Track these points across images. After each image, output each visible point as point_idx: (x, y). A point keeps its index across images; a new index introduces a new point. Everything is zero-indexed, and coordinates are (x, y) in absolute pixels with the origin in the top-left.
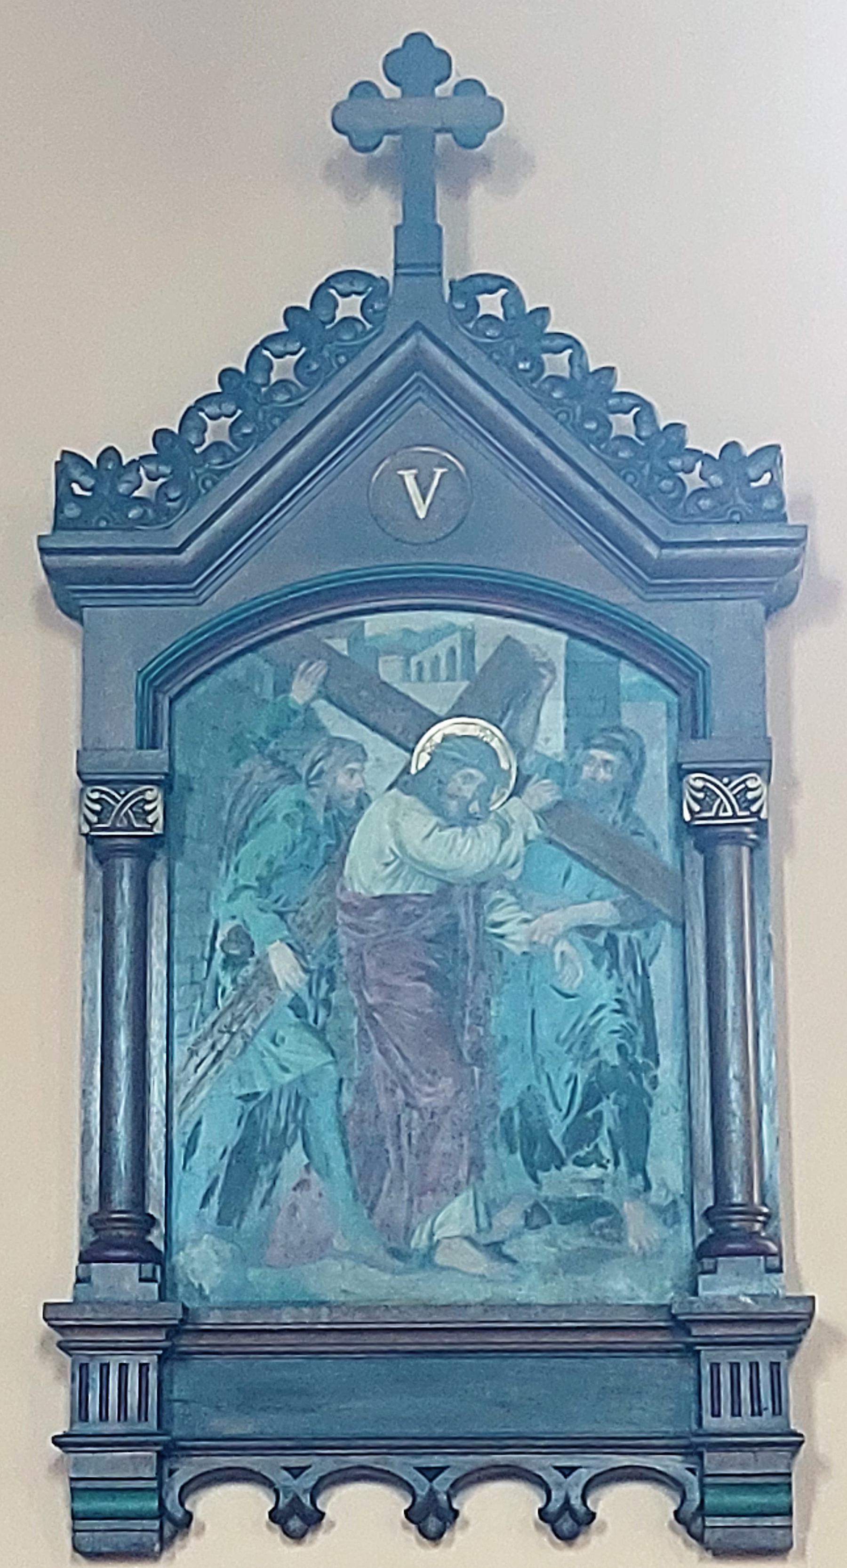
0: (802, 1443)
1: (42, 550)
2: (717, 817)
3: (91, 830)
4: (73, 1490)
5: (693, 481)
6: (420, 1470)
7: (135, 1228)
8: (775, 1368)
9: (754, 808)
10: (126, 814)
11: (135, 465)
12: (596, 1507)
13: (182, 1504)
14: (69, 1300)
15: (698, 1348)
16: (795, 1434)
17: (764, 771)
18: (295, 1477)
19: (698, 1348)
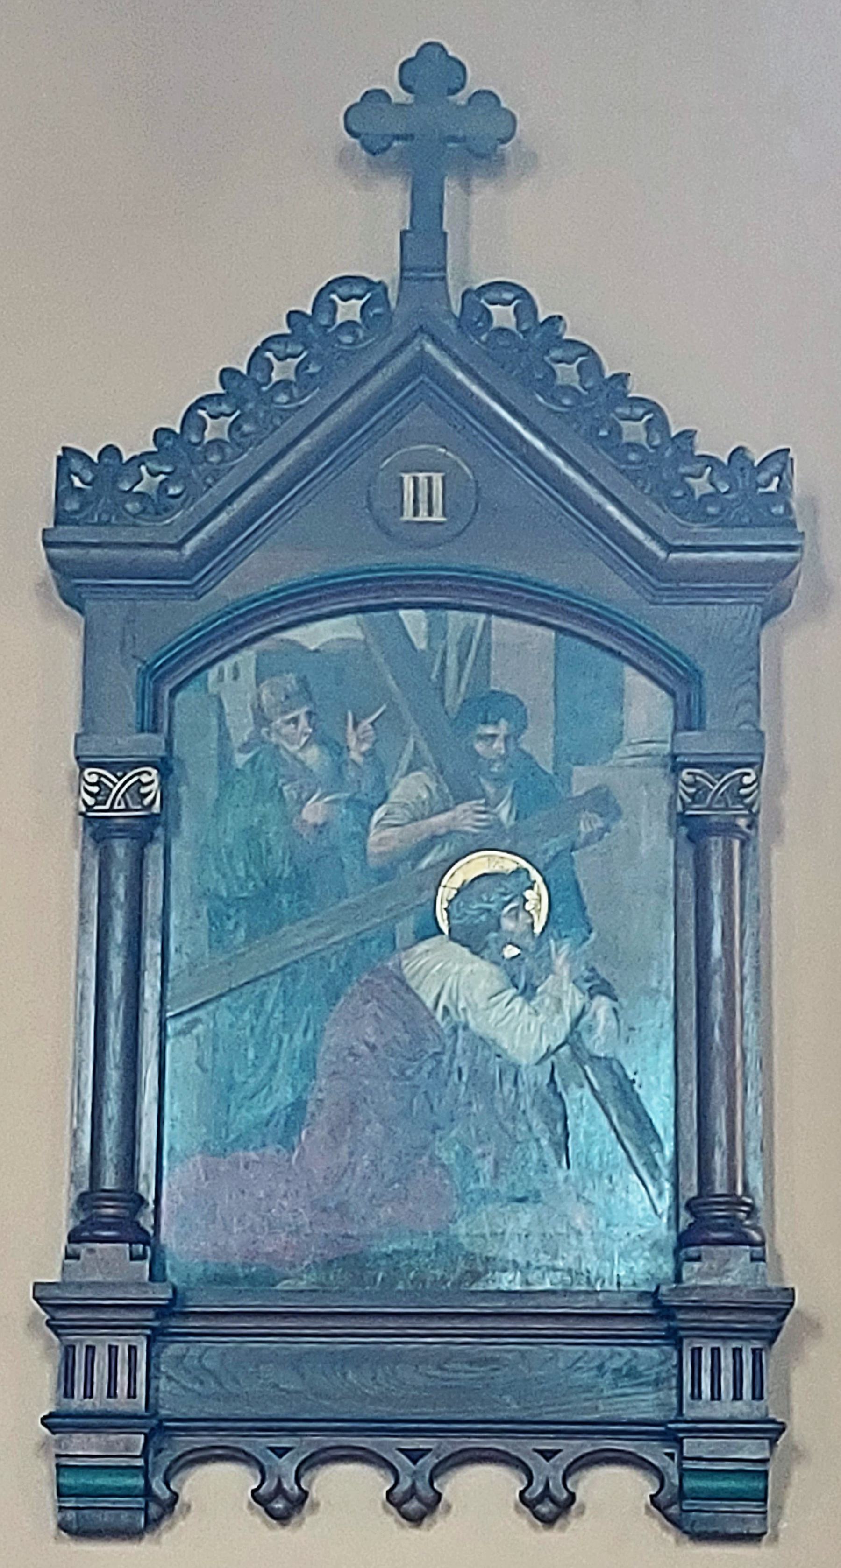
0: (784, 1430)
1: (47, 544)
2: (111, 809)
3: (87, 811)
4: (58, 1466)
5: (701, 486)
7: (124, 1208)
9: (147, 801)
11: (135, 462)
13: (167, 1484)
14: (57, 1279)
16: (773, 1421)
18: (548, 1459)
19: (682, 1333)
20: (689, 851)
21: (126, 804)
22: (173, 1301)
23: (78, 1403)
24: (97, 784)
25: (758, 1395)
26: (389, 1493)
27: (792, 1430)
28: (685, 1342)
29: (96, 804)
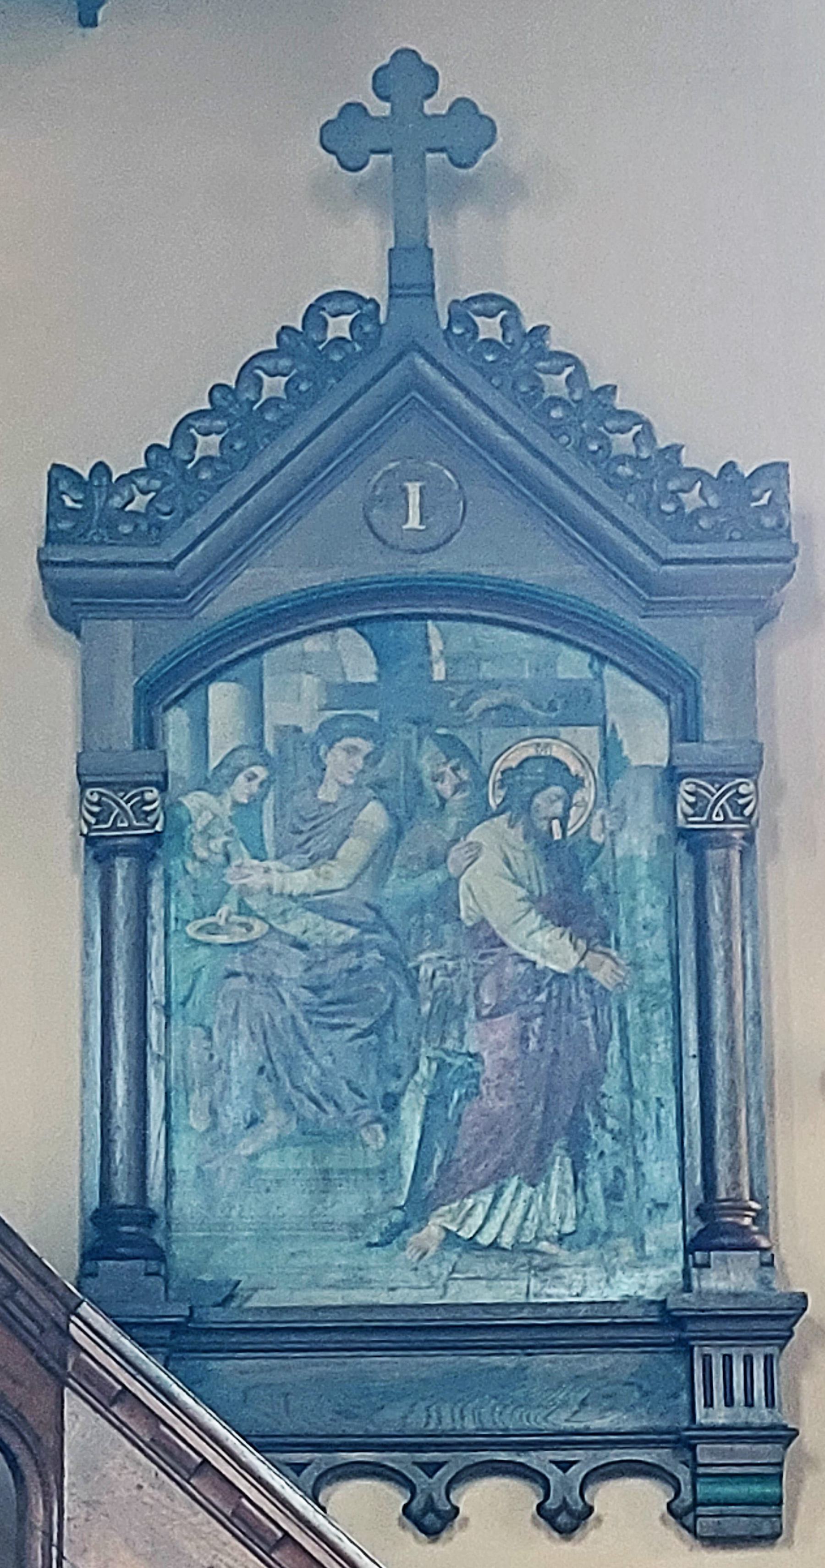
0: (798, 1434)
5: (692, 500)
8: (748, 1359)
10: (722, 806)
12: (458, 1501)
15: (692, 1343)
16: (785, 1428)
19: (692, 1343)
20: (96, 871)
22: (190, 1318)
24: (98, 804)
25: (770, 1403)
26: (406, 1507)
27: (803, 1437)
28: (696, 1349)
29: (97, 823)
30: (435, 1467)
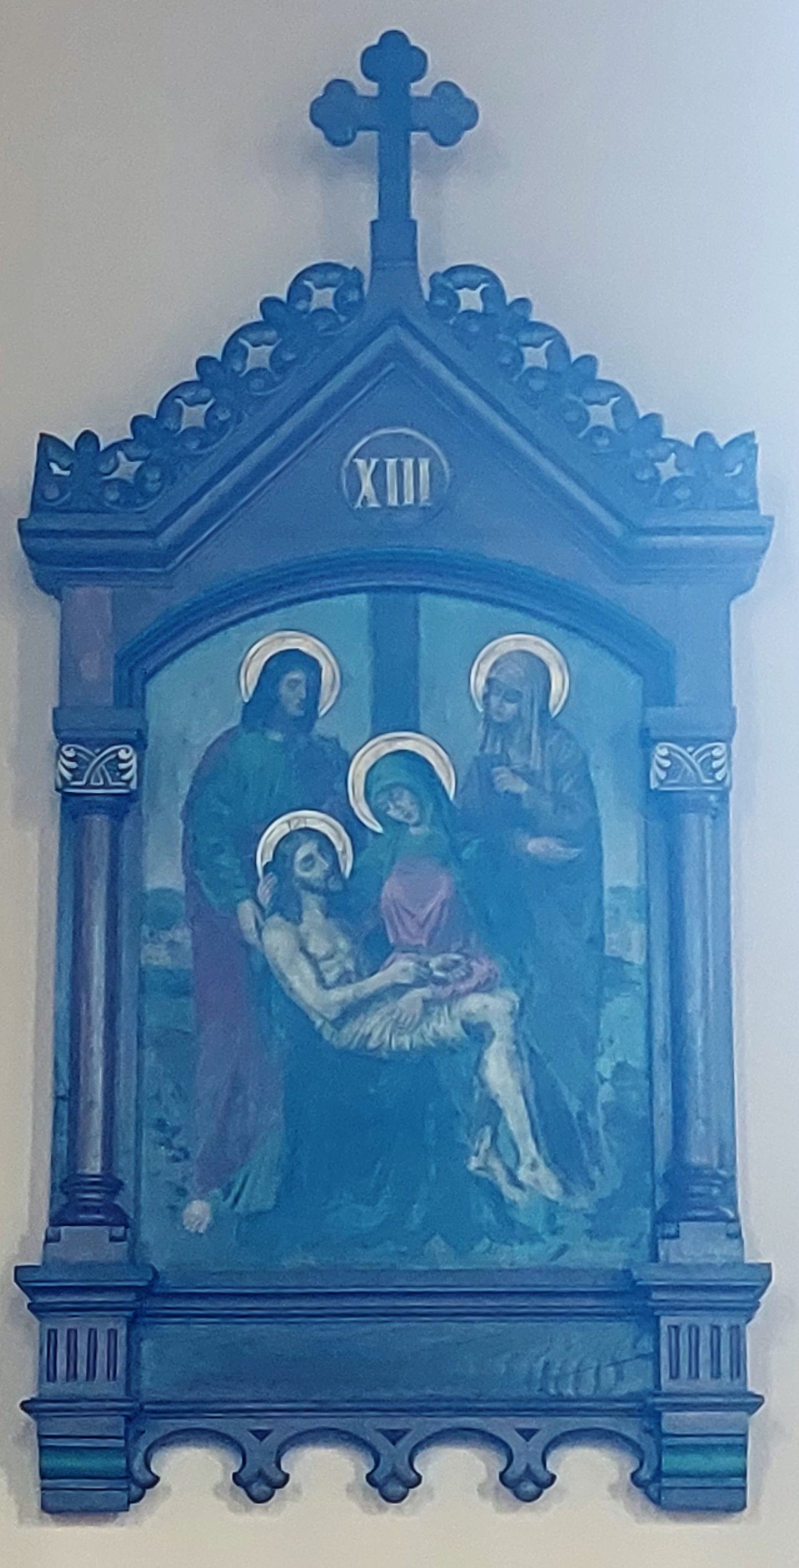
2: (87, 786)
5: (668, 469)
6: (384, 1432)
8: (72, 1335)
13: (148, 1466)
15: (657, 1313)
17: (728, 740)
21: (105, 780)
22: (152, 1284)
23: (60, 1387)
29: (667, 777)
30: (258, 1434)
